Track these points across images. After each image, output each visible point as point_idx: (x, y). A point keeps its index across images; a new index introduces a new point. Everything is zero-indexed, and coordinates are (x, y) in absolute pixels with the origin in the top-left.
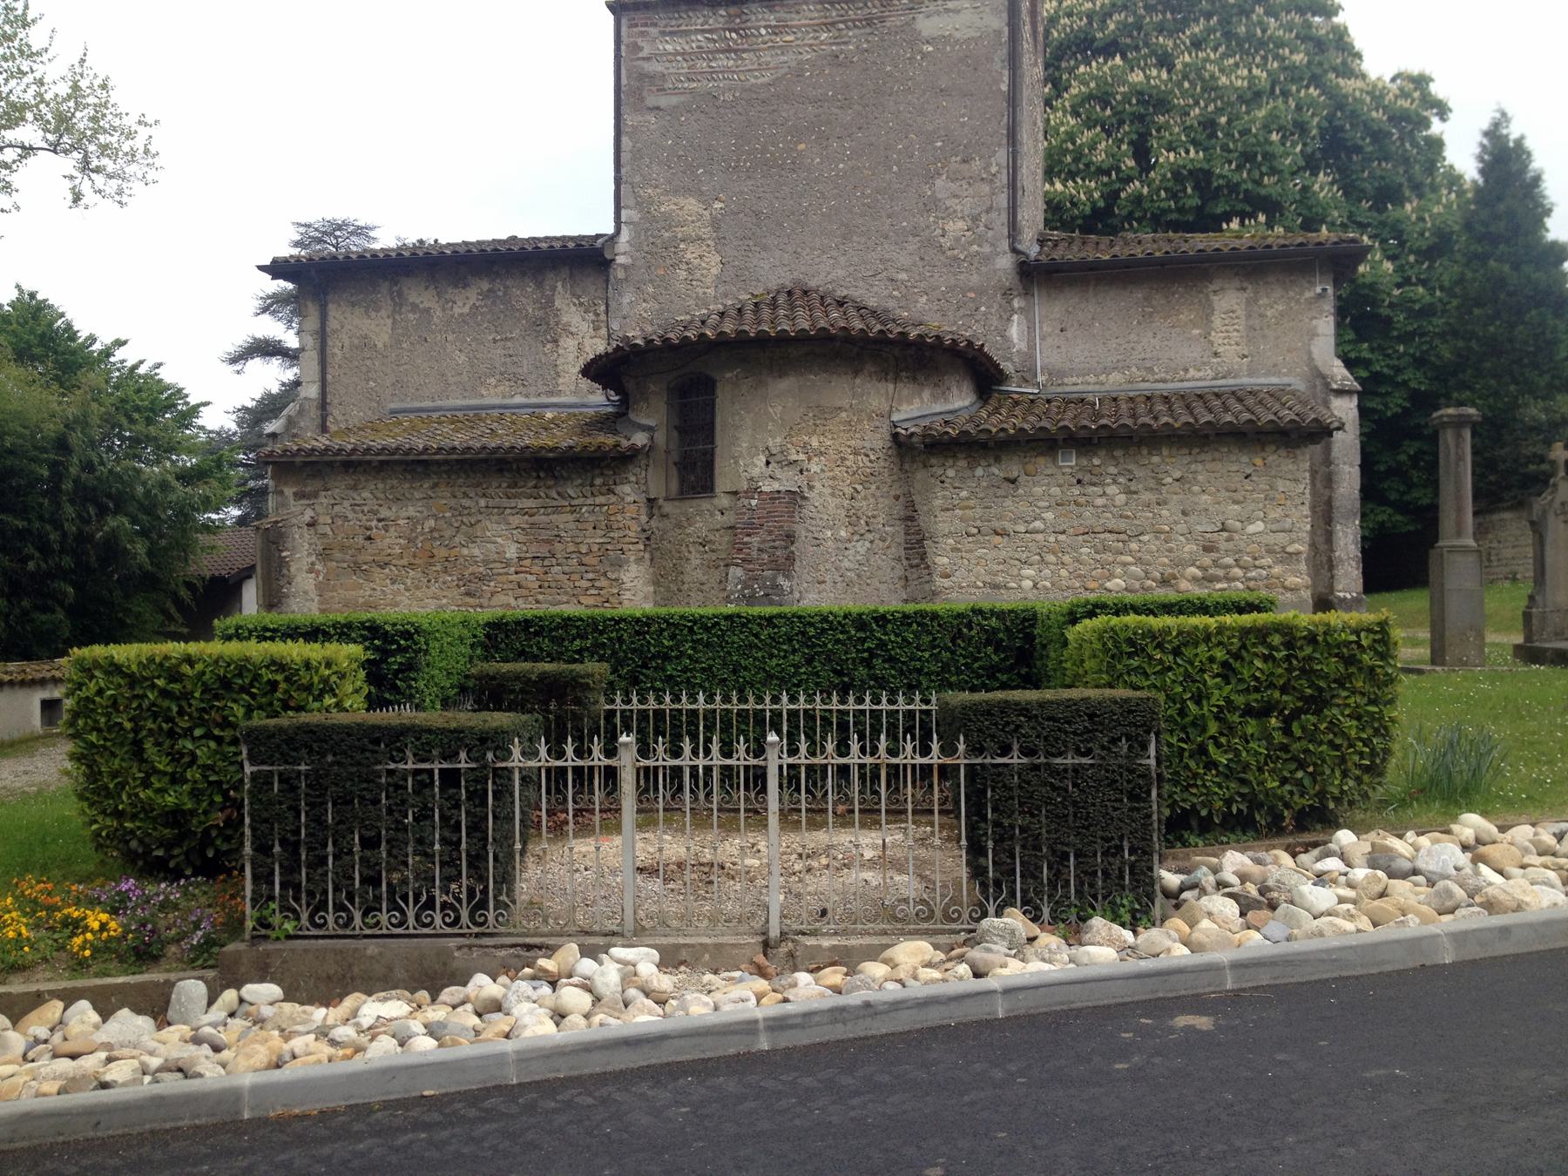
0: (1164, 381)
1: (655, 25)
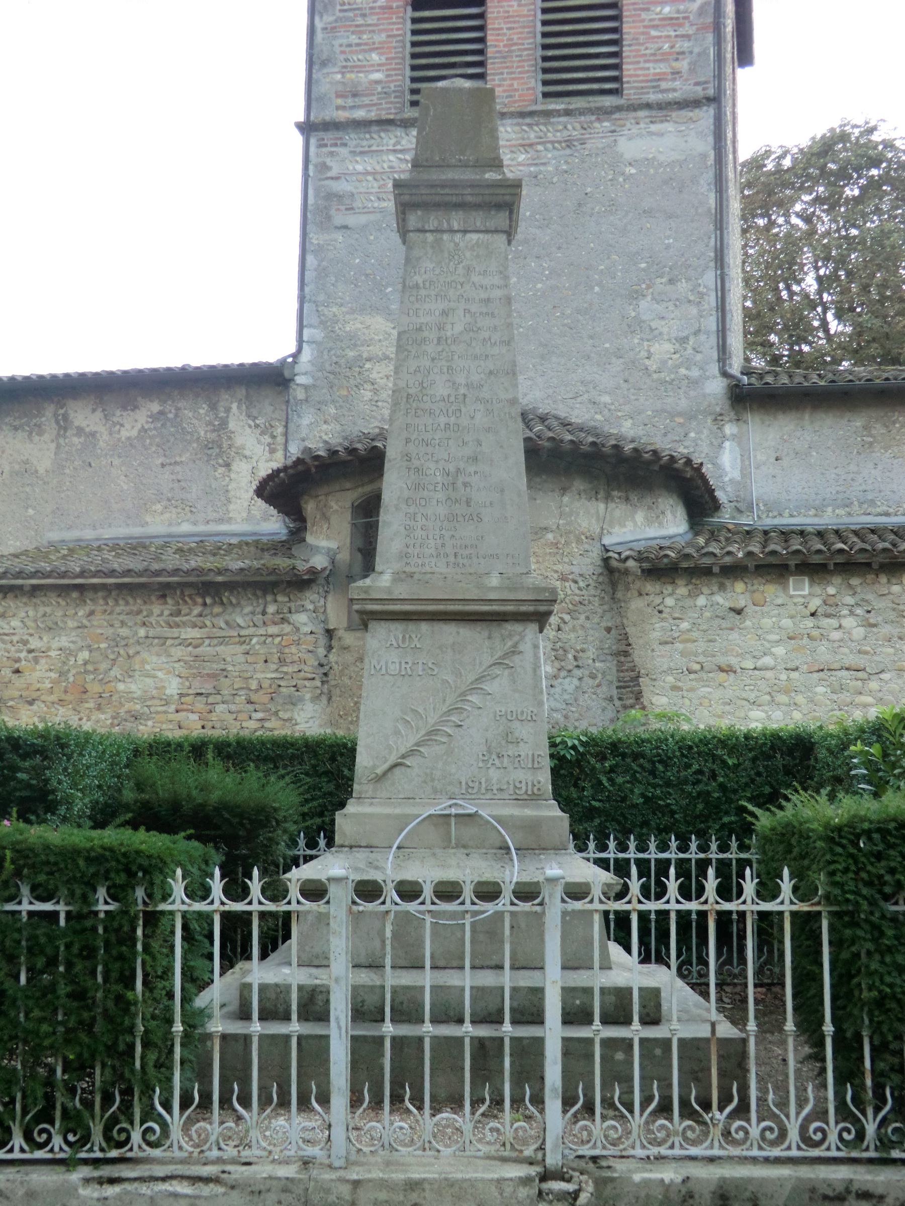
0: (887, 514)
1: (345, 145)
